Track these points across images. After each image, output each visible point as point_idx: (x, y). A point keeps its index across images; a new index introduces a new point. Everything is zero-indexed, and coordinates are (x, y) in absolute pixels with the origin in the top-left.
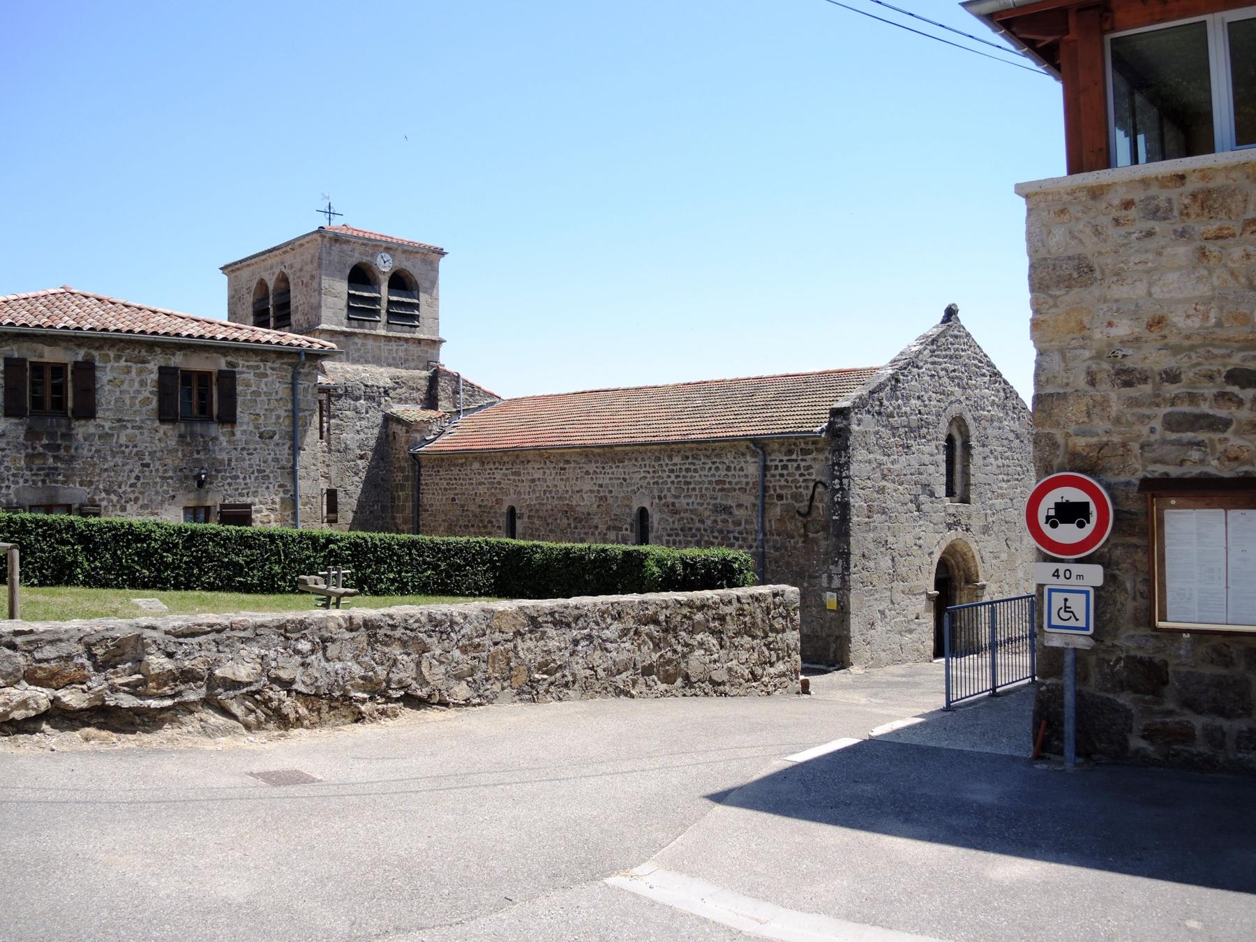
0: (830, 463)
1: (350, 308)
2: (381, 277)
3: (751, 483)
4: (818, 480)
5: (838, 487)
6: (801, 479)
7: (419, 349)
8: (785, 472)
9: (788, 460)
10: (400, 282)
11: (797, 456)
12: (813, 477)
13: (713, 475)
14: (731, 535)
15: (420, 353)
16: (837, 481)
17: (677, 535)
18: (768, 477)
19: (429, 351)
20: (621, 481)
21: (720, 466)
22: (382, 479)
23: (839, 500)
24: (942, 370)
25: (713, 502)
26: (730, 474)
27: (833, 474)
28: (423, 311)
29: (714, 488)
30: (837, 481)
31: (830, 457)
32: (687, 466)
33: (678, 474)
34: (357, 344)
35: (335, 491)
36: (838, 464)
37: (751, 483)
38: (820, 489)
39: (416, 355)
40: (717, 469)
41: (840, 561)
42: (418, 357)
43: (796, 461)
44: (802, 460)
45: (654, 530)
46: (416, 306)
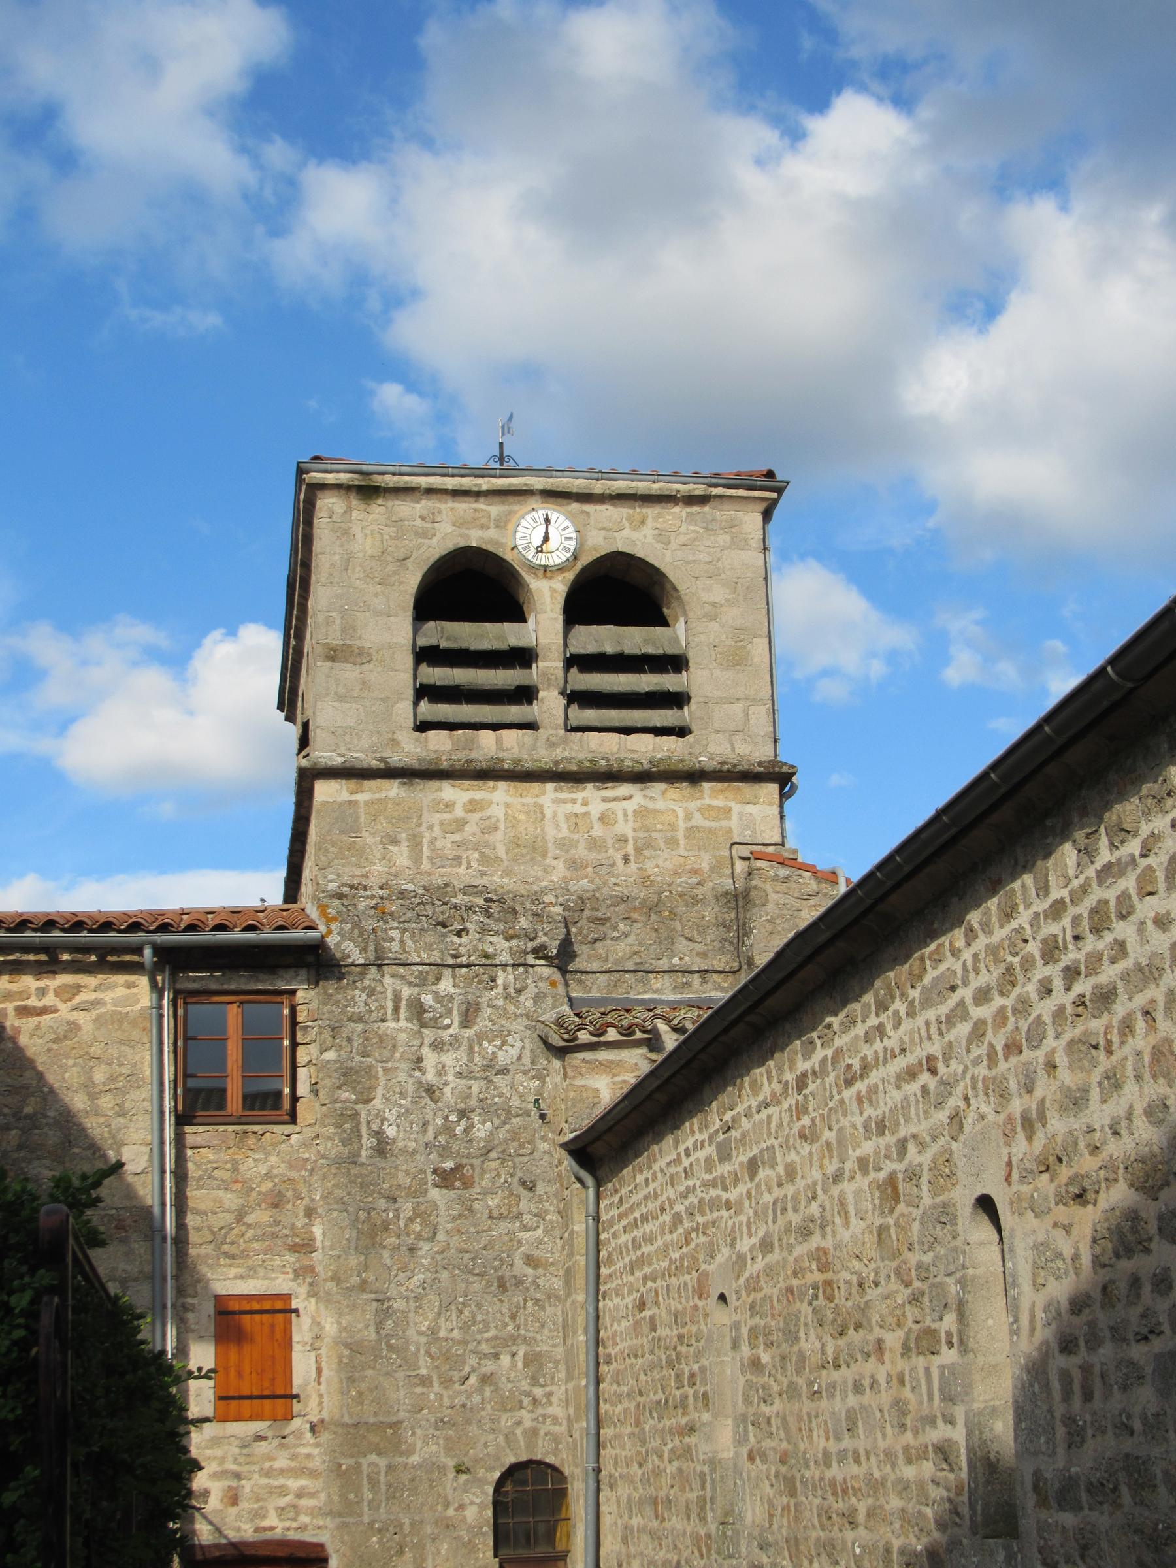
7: (693, 805)
15: (698, 820)
17: (1094, 1341)
19: (736, 808)
20: (925, 1078)
22: (530, 1261)
34: (449, 806)
42: (691, 831)
46: (675, 663)
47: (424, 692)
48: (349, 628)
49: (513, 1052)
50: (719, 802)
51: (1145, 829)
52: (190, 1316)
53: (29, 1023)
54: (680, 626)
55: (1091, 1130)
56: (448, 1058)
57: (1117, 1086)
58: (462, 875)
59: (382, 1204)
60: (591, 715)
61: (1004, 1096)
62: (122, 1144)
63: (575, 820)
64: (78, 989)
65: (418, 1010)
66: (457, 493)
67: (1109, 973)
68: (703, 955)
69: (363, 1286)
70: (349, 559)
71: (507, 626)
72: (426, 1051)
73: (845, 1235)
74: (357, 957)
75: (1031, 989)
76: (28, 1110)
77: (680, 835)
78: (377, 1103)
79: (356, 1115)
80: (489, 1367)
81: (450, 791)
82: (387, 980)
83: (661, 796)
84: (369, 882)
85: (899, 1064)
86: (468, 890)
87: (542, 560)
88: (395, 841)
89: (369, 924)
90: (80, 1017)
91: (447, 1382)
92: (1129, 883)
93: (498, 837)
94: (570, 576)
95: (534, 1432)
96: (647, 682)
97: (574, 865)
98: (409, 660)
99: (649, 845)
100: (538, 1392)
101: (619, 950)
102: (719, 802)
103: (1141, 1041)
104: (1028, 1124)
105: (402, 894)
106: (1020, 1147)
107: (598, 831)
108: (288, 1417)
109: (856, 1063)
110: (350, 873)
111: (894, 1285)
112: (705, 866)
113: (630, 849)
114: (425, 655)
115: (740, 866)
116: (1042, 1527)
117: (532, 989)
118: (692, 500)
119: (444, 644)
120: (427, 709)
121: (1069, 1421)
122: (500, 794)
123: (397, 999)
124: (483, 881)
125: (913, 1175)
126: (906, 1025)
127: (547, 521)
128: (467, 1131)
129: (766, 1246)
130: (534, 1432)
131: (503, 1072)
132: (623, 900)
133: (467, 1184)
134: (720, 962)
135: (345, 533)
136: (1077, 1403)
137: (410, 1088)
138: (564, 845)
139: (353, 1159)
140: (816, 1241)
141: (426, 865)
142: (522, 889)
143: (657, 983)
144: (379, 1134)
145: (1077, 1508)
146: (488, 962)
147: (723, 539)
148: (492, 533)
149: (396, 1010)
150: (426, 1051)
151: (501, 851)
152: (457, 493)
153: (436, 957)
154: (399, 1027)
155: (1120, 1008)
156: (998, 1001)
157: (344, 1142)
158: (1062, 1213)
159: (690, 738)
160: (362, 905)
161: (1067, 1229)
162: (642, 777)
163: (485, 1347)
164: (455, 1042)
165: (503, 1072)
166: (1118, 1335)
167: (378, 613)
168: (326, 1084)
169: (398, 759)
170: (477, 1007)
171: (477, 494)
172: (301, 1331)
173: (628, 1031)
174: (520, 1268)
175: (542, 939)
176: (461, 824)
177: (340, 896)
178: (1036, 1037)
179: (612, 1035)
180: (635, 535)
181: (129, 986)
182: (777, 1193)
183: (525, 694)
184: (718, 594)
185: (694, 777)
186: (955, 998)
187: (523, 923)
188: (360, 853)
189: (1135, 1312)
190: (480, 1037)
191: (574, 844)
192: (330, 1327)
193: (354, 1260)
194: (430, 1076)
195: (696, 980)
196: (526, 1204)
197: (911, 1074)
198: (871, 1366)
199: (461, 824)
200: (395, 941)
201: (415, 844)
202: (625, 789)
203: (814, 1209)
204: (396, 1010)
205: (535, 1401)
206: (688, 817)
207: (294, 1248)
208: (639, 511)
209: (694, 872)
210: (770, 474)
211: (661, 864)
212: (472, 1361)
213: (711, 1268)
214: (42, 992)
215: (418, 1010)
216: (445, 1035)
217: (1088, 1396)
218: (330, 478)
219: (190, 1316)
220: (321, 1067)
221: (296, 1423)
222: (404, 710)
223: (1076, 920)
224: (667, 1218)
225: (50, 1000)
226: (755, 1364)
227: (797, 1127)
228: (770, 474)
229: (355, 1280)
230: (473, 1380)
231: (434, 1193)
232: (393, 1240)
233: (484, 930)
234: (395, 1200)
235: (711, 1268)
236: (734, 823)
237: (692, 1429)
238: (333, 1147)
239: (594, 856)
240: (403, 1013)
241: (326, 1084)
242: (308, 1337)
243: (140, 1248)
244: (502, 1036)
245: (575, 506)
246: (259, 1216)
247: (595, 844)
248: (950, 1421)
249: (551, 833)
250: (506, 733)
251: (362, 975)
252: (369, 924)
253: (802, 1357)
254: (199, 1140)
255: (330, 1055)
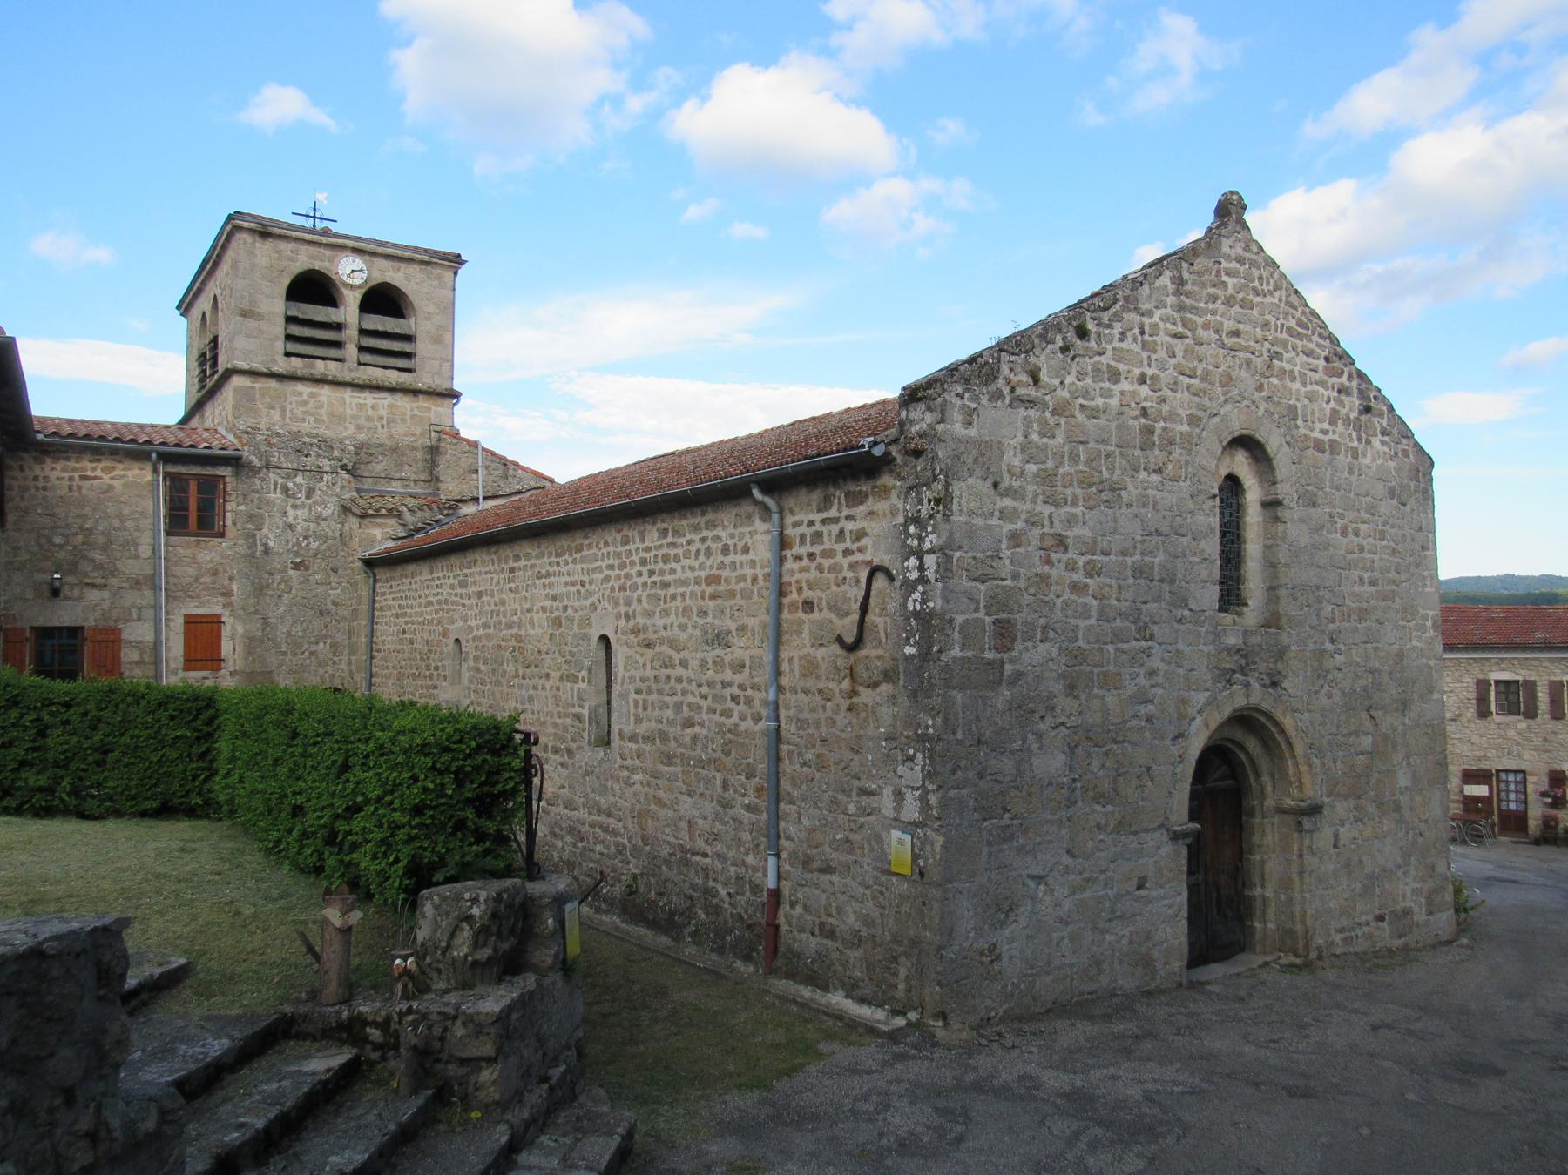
0: (901, 519)
1: (289, 338)
2: (346, 292)
3: (761, 577)
4: (876, 561)
5: (914, 575)
6: (846, 562)
7: (414, 405)
8: (817, 549)
9: (824, 521)
10: (382, 300)
11: (840, 510)
12: (868, 557)
13: (702, 567)
14: (727, 692)
15: (416, 412)
16: (913, 561)
17: (649, 692)
18: (790, 565)
19: (433, 408)
20: (579, 587)
21: (714, 546)
22: (334, 603)
23: (918, 607)
24: (1206, 326)
25: (701, 622)
26: (728, 560)
27: (905, 545)
28: (422, 347)
29: (703, 592)
30: (913, 561)
31: (900, 505)
32: (665, 550)
33: (652, 567)
34: (300, 394)
35: (215, 622)
36: (916, 520)
37: (761, 577)
38: (880, 582)
39: (409, 414)
40: (708, 552)
41: (919, 756)
42: (412, 417)
43: (836, 520)
44: (848, 518)
45: (619, 680)
46: (409, 338)
47: (289, 337)
48: (252, 302)
49: (330, 511)
50: (426, 405)
51: (688, 537)
52: (172, 624)
53: (86, 484)
54: (412, 320)
55: (654, 625)
56: (299, 512)
57: (668, 615)
58: (306, 427)
59: (266, 576)
60: (368, 358)
61: (617, 604)
62: (137, 544)
63: (360, 407)
64: (113, 468)
65: (286, 490)
66: (310, 242)
67: (667, 578)
68: (415, 473)
69: (256, 612)
70: (253, 268)
71: (330, 309)
72: (289, 508)
73: (532, 632)
74: (256, 462)
75: (633, 572)
76: (87, 526)
77: (408, 417)
78: (265, 530)
79: (255, 535)
80: (314, 648)
81: (304, 389)
82: (271, 475)
83: (403, 402)
84: (261, 427)
85: (563, 579)
86: (309, 435)
87: (350, 281)
88: (272, 408)
89: (263, 448)
90: (115, 483)
91: (295, 654)
92: (680, 551)
93: (323, 411)
94: (363, 291)
95: (333, 676)
96: (396, 346)
97: (358, 427)
98: (283, 321)
99: (393, 421)
100: (335, 659)
101: (378, 468)
102: (426, 405)
103: (678, 602)
104: (627, 616)
105: (278, 434)
106: (622, 622)
107: (370, 412)
108: (219, 669)
109: (544, 572)
110: (251, 421)
111: (557, 655)
112: (418, 433)
113: (385, 422)
114: (290, 320)
115: (433, 434)
116: (620, 747)
117: (339, 484)
118: (422, 262)
119: (300, 316)
120: (292, 347)
121: (636, 715)
122: (325, 392)
123: (276, 484)
124: (315, 431)
125: (571, 620)
126: (571, 566)
127: (361, 271)
128: (307, 545)
129: (486, 626)
130: (333, 676)
131: (324, 520)
132: (381, 445)
133: (307, 569)
134: (423, 477)
135: (252, 253)
136: (640, 710)
137: (281, 525)
138: (354, 417)
139: (253, 555)
140: (515, 631)
141: (288, 421)
142: (334, 436)
143: (394, 484)
144: (265, 545)
145: (637, 742)
146: (320, 471)
147: (435, 283)
148: (326, 264)
149: (275, 489)
150: (289, 508)
151: (325, 418)
152: (310, 242)
153: (295, 466)
154: (276, 497)
155: (671, 590)
156: (617, 572)
157: (249, 548)
158: (639, 649)
159: (414, 374)
160: (259, 438)
161: (642, 655)
162: (392, 390)
163: (312, 639)
164: (303, 505)
165: (324, 520)
166: (660, 692)
167: (267, 296)
168: (241, 520)
169: (275, 369)
170: (314, 490)
171: (320, 244)
172: (226, 632)
173: (390, 510)
174: (330, 606)
175: (345, 461)
176: (305, 403)
177: (247, 433)
178: (634, 587)
179: (384, 512)
180: (394, 275)
181: (141, 469)
182: (493, 607)
183: (338, 345)
184: (431, 309)
185: (416, 392)
186: (598, 564)
187: (336, 453)
188: (257, 413)
189: (667, 687)
190: (315, 503)
191: (359, 417)
192: (240, 630)
193: (252, 601)
194: (290, 520)
195: (412, 484)
196: (334, 579)
197: (573, 584)
198: (542, 681)
199: (305, 403)
200: (276, 457)
201: (283, 410)
202: (383, 395)
203: (515, 618)
204: (275, 489)
205: (334, 663)
206: (412, 410)
207: (223, 594)
208: (397, 264)
209: (413, 435)
210: (459, 256)
211: (399, 430)
212: (306, 646)
213: (451, 627)
214: (94, 469)
215: (286, 490)
216: (298, 502)
217: (645, 709)
218: (246, 224)
219: (172, 624)
220: (237, 513)
221: (223, 671)
222: (280, 345)
223: (656, 556)
224: (423, 601)
225: (98, 473)
226: (478, 670)
227: (508, 586)
228: (459, 256)
229: (253, 609)
230: (307, 654)
231: (291, 572)
232: (271, 592)
233: (319, 456)
234: (272, 574)
235: (451, 627)
236: (432, 415)
237: (435, 687)
238: (243, 550)
239: (368, 424)
240: (278, 490)
241: (241, 520)
242: (229, 634)
243: (148, 593)
244: (325, 504)
245: (367, 257)
246: (207, 579)
247: (369, 419)
248: (582, 707)
249: (348, 411)
250: (329, 362)
251: (259, 472)
252: (263, 448)
253: (505, 672)
254: (175, 544)
255: (242, 508)
